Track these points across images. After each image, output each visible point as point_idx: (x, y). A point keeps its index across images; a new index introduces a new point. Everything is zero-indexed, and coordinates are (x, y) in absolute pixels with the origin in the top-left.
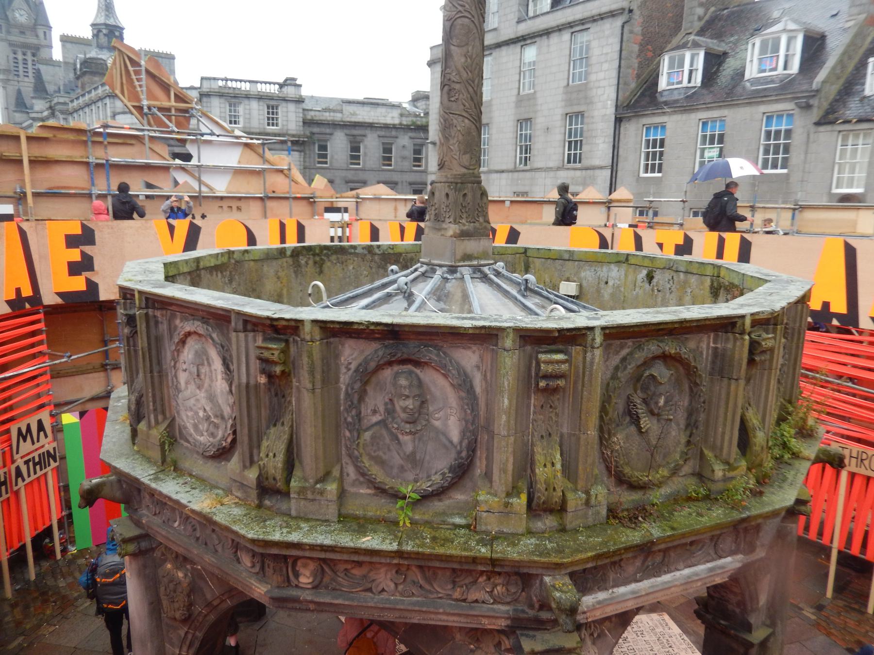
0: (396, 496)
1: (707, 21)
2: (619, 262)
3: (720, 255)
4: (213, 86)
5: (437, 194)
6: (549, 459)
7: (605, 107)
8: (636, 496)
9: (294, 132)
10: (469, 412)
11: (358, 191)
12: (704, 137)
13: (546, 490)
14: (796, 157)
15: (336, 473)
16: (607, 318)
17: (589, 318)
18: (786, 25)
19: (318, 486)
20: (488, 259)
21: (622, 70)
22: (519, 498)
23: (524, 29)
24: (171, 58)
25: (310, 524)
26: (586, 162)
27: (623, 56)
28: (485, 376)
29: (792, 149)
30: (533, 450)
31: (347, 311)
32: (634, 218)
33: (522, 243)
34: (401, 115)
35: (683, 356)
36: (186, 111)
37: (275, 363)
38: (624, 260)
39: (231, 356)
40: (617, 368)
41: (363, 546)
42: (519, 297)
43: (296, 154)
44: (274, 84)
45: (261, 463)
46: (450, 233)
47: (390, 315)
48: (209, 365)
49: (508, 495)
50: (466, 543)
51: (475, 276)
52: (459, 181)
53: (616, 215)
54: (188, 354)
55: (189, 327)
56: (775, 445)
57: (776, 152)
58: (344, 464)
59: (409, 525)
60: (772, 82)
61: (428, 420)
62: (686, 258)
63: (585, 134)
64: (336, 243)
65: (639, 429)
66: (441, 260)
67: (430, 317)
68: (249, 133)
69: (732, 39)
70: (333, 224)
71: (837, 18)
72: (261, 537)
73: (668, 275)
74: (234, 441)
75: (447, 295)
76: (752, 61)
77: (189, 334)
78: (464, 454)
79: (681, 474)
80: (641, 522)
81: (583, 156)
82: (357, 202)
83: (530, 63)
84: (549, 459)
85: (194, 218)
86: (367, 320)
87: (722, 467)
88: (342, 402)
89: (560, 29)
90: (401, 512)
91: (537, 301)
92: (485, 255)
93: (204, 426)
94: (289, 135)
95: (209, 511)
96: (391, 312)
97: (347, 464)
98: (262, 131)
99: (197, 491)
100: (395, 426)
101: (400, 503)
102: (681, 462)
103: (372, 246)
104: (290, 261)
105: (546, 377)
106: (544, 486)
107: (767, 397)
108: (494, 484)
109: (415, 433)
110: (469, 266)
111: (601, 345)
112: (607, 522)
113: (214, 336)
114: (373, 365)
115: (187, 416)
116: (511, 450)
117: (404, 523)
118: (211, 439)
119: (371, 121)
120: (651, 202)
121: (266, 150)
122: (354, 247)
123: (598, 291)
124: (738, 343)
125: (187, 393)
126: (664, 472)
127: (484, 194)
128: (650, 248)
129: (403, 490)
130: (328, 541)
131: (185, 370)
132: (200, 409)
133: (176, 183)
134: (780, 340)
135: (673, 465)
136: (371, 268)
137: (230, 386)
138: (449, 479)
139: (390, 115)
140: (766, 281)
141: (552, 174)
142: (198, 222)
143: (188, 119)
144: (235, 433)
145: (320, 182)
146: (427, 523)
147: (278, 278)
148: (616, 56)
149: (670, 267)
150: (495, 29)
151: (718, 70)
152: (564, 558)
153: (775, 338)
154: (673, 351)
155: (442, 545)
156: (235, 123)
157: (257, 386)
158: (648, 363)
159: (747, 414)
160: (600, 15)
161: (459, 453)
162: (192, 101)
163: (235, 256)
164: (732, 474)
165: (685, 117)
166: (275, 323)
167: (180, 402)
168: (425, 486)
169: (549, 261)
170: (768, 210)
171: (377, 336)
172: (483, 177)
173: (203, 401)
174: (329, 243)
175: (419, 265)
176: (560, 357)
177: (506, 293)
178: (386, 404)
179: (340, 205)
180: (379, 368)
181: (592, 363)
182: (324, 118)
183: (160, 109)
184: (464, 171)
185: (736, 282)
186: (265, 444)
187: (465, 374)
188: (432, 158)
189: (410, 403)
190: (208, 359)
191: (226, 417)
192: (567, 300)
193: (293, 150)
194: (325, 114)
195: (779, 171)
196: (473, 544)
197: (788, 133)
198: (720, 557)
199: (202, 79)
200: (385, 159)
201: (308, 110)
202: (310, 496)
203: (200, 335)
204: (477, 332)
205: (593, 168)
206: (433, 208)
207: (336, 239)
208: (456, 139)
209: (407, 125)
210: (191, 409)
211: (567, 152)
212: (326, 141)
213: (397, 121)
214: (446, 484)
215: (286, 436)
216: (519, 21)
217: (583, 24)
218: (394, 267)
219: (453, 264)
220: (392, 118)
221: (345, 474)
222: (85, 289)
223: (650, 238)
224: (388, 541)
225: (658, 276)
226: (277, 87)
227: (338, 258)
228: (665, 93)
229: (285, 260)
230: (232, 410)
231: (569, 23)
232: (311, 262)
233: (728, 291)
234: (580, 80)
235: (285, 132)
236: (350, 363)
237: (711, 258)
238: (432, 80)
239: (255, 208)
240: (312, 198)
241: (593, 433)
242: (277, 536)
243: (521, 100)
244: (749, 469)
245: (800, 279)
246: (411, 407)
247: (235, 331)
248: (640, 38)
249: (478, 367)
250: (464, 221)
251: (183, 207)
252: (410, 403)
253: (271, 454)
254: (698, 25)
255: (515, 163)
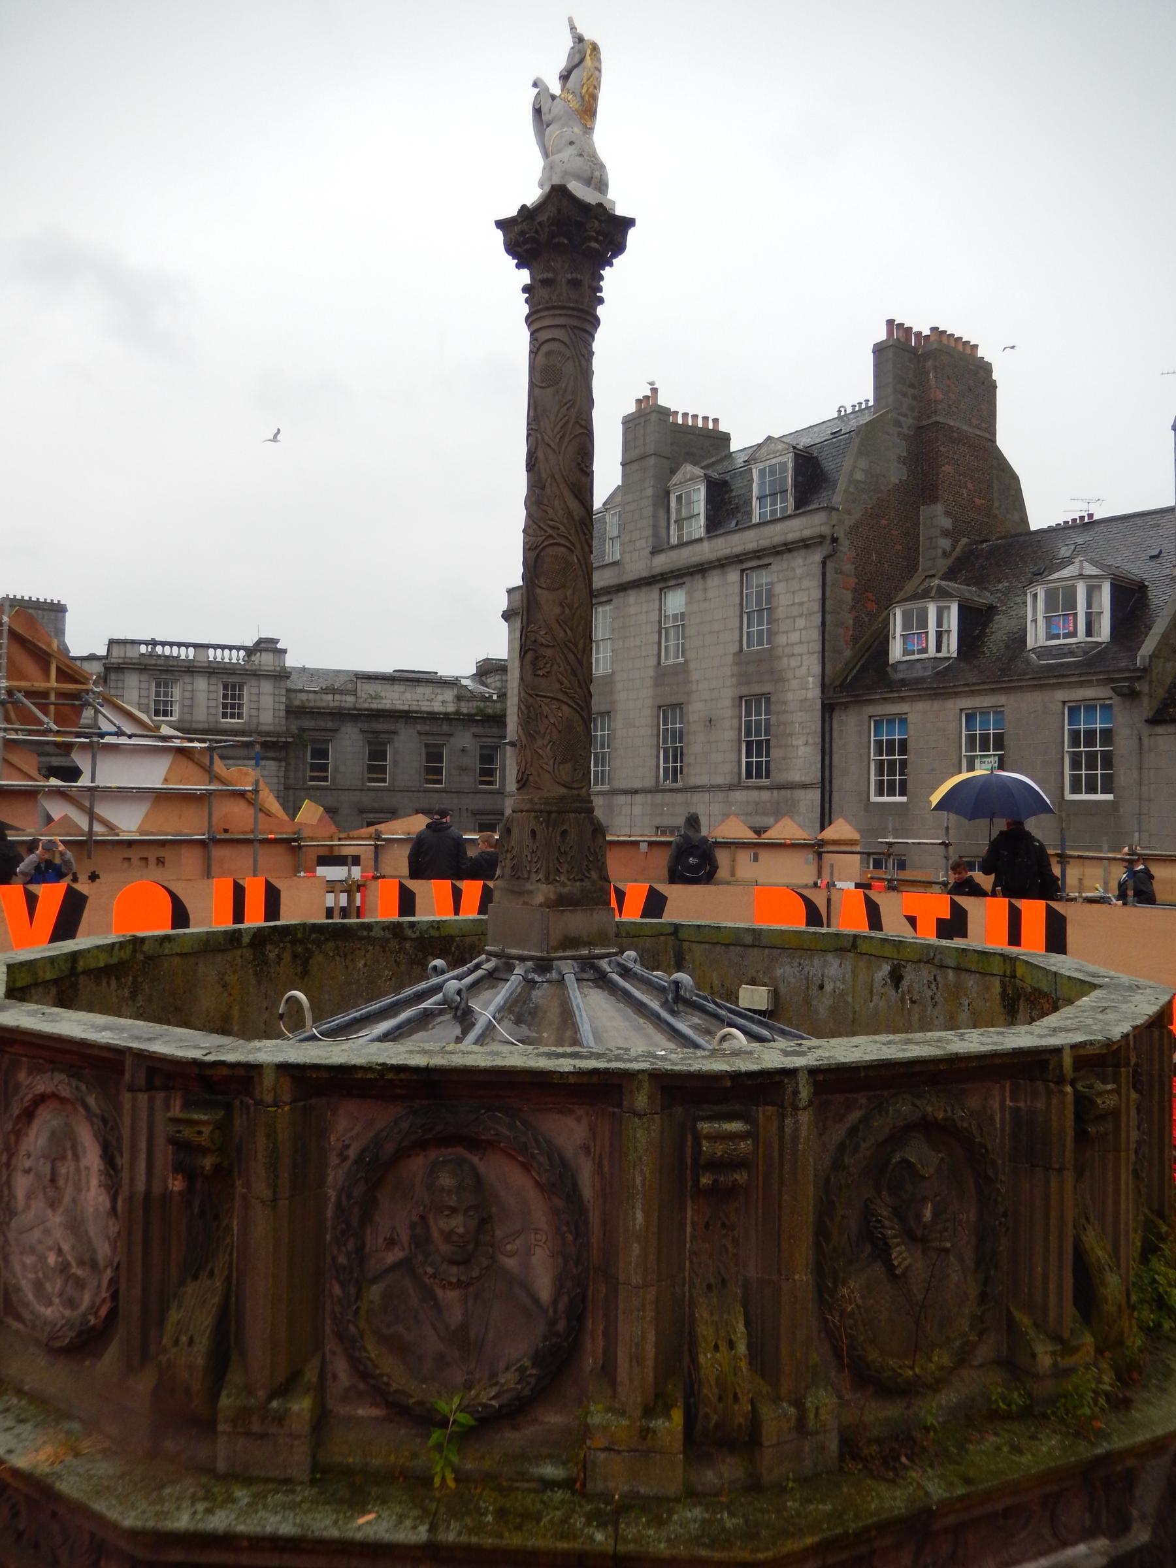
0: (428, 1420)
1: (958, 559)
2: (842, 949)
3: (1015, 938)
4: (129, 655)
5: (515, 831)
6: (723, 1334)
7: (804, 687)
8: (892, 1411)
9: (271, 728)
10: (570, 1237)
11: (380, 827)
12: (971, 739)
13: (720, 1399)
14: (1124, 775)
15: (311, 1375)
16: (819, 1052)
17: (786, 1053)
18: (1082, 568)
19: (275, 1404)
20: (608, 946)
21: (827, 628)
22: (669, 1417)
23: (662, 562)
24: (58, 610)
25: (255, 1489)
26: (778, 777)
27: (828, 608)
28: (600, 1165)
29: (1116, 761)
30: (692, 1315)
31: (346, 1046)
32: (863, 873)
33: (670, 916)
34: (459, 698)
35: (959, 1124)
36: (76, 696)
37: (203, 1151)
38: (848, 946)
39: (119, 1139)
40: (841, 1148)
41: (359, 1536)
42: (664, 1014)
43: (271, 766)
44: (238, 648)
45: (163, 1358)
46: (539, 899)
47: (425, 1052)
48: (76, 1157)
49: (649, 1412)
50: (565, 1520)
51: (585, 976)
52: (554, 808)
53: (832, 866)
54: (36, 1139)
55: (42, 1084)
56: (1142, 1301)
57: (1091, 766)
58: (328, 1354)
59: (451, 1484)
60: (1071, 653)
61: (492, 1257)
62: (958, 943)
63: (773, 730)
64: (337, 920)
65: (890, 1268)
66: (524, 949)
67: (498, 1054)
68: (186, 730)
69: (1000, 586)
70: (332, 886)
71: (1160, 560)
72: (150, 1524)
73: (926, 973)
74: (113, 1314)
75: (534, 1013)
76: (1035, 621)
77: (41, 1099)
78: (561, 1326)
79: (975, 1363)
80: (905, 1468)
81: (772, 766)
82: (376, 846)
83: (675, 616)
84: (723, 1334)
85: (75, 880)
86: (381, 1061)
87: (1050, 1348)
88: (329, 1224)
89: (722, 564)
90: (437, 1456)
91: (696, 1020)
92: (601, 938)
93: (54, 1286)
94: (260, 733)
95: (47, 1470)
96: (427, 1046)
97: (334, 1353)
98: (212, 726)
99: (28, 1427)
100: (430, 1270)
101: (437, 1436)
102: (973, 1338)
103: (399, 924)
104: (248, 954)
105: (714, 1165)
106: (716, 1391)
107: (1117, 1203)
108: (620, 1389)
109: (468, 1285)
110: (573, 958)
111: (811, 1103)
112: (841, 1469)
113: (91, 1100)
114: (390, 1148)
115: (24, 1265)
116: (650, 1314)
117: (443, 1479)
118: (67, 1313)
119: (406, 708)
120: (890, 844)
121: (216, 758)
122: (368, 927)
123: (807, 1002)
124: (1055, 1101)
125: (29, 1217)
126: (942, 1358)
127: (599, 830)
128: (894, 926)
129: (443, 1406)
130: (286, 1527)
131: (28, 1171)
132: (50, 1249)
133: (49, 819)
134: (1128, 1096)
135: (958, 1343)
136: (398, 964)
137: (114, 1200)
138: (533, 1381)
139: (440, 698)
140: (1095, 987)
141: (720, 796)
142: (83, 887)
143: (78, 711)
144: (115, 1296)
145: (310, 813)
146: (489, 1479)
147: (225, 986)
148: (816, 607)
149: (929, 957)
150: (615, 563)
151: (983, 634)
152: (758, 1550)
153: (1117, 1091)
154: (941, 1115)
155: (519, 1528)
156: (165, 714)
157: (166, 1196)
158: (898, 1137)
159: (1084, 1238)
160: (785, 544)
161: (552, 1323)
162: (88, 679)
163: (146, 948)
164: (1069, 1361)
165: (937, 705)
166: (208, 1072)
167: (11, 1235)
168: (486, 1396)
169: (718, 948)
170: (1087, 862)
171: (399, 1091)
172: (598, 802)
173: (58, 1233)
174: (323, 920)
175: (484, 956)
176: (736, 1126)
177: (640, 1008)
178: (413, 1226)
179: (346, 851)
180: (403, 1153)
181: (795, 1138)
182: (324, 704)
183: (29, 694)
184: (563, 791)
185: (1044, 986)
186: (174, 1316)
187: (564, 1164)
188: (510, 766)
189: (457, 1224)
190: (74, 1148)
191: (102, 1263)
192: (751, 1020)
193: (268, 759)
194: (326, 697)
195: (1100, 797)
196: (579, 1522)
197: (1107, 736)
198: (1065, 1544)
199: (112, 642)
200: (429, 771)
201: (296, 691)
202: (256, 1428)
203: (63, 1100)
204: (584, 1080)
205: (792, 786)
206: (509, 856)
207: (336, 912)
208: (547, 738)
209: (470, 715)
210: (33, 1251)
211: (744, 760)
212: (327, 742)
213: (451, 708)
214: (526, 1392)
215: (216, 1300)
216: (655, 551)
217: (759, 558)
218: (438, 962)
219: (545, 954)
220: (442, 702)
221: (329, 1376)
222: (949, 917)
223: (893, 907)
224: (408, 1523)
225: (910, 976)
226: (242, 653)
227: (337, 948)
228: (901, 667)
229: (239, 952)
230: (114, 1249)
231: (737, 556)
232: (287, 956)
233: (1032, 1002)
234: (760, 643)
235: (253, 727)
236: (347, 1147)
237: (1000, 945)
238: (510, 641)
239: (190, 860)
240: (295, 840)
241: (803, 1277)
242: (183, 1522)
243: (662, 674)
244: (1100, 1351)
245: (1151, 983)
246: (461, 1230)
247: (131, 1089)
248: (852, 581)
249: (586, 1149)
250: (563, 878)
251: (57, 861)
252: (457, 1224)
253: (184, 1339)
254: (943, 564)
255: (658, 777)
